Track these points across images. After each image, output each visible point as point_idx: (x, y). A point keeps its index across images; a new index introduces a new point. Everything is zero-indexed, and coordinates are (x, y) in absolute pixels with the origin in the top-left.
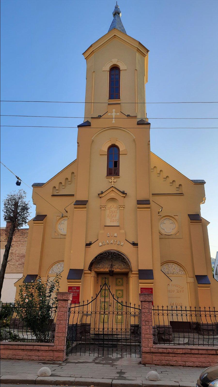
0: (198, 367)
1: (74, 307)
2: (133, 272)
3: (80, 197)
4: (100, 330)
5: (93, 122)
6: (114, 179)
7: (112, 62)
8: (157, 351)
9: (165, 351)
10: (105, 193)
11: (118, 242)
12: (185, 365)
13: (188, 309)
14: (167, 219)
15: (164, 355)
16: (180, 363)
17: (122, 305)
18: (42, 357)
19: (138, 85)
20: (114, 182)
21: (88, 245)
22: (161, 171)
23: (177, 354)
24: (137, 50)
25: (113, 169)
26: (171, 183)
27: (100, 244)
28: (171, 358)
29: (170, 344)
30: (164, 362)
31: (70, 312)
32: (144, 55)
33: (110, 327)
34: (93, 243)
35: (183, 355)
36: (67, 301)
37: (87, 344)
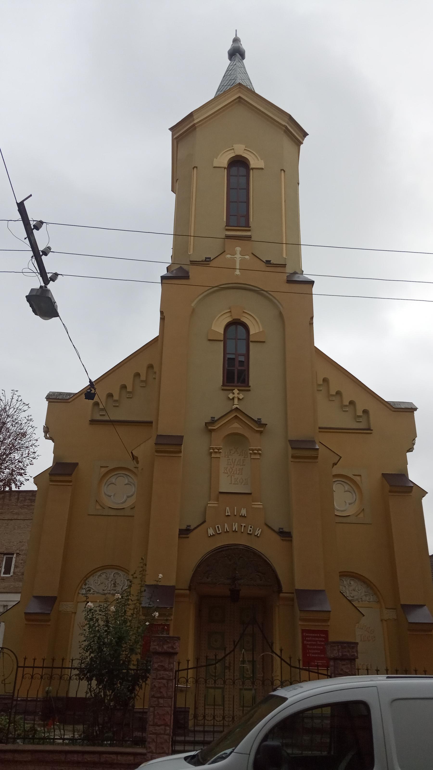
2: (282, 595)
3: (165, 427)
5: (193, 271)
6: (238, 392)
7: (232, 151)
17: (290, 665)
20: (239, 399)
27: (211, 532)
31: (178, 681)
32: (299, 143)
34: (195, 528)
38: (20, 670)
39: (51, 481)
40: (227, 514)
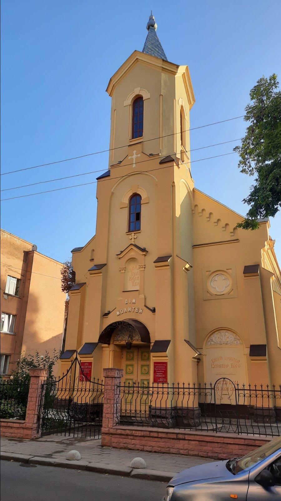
0: (157, 452)
1: (121, 387)
4: (122, 411)
8: (115, 432)
9: (123, 432)
10: (124, 252)
11: (137, 309)
12: (143, 449)
13: (247, 387)
14: (218, 275)
15: (123, 436)
16: (138, 447)
18: (14, 434)
19: (163, 114)
20: (134, 238)
21: (106, 315)
22: (211, 214)
23: (136, 436)
24: (162, 70)
25: (135, 219)
26: (223, 227)
27: (118, 313)
28: (130, 441)
29: (191, 430)
30: (122, 445)
33: (133, 408)
35: (142, 438)
36: (38, 378)
37: (96, 425)
38: (237, 391)
39: (245, 277)
40: (126, 303)
